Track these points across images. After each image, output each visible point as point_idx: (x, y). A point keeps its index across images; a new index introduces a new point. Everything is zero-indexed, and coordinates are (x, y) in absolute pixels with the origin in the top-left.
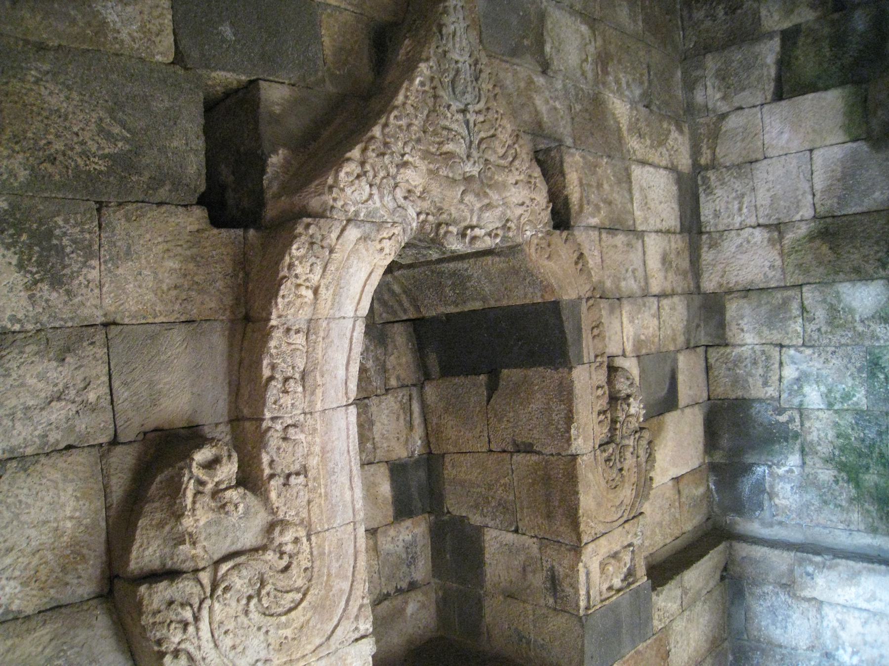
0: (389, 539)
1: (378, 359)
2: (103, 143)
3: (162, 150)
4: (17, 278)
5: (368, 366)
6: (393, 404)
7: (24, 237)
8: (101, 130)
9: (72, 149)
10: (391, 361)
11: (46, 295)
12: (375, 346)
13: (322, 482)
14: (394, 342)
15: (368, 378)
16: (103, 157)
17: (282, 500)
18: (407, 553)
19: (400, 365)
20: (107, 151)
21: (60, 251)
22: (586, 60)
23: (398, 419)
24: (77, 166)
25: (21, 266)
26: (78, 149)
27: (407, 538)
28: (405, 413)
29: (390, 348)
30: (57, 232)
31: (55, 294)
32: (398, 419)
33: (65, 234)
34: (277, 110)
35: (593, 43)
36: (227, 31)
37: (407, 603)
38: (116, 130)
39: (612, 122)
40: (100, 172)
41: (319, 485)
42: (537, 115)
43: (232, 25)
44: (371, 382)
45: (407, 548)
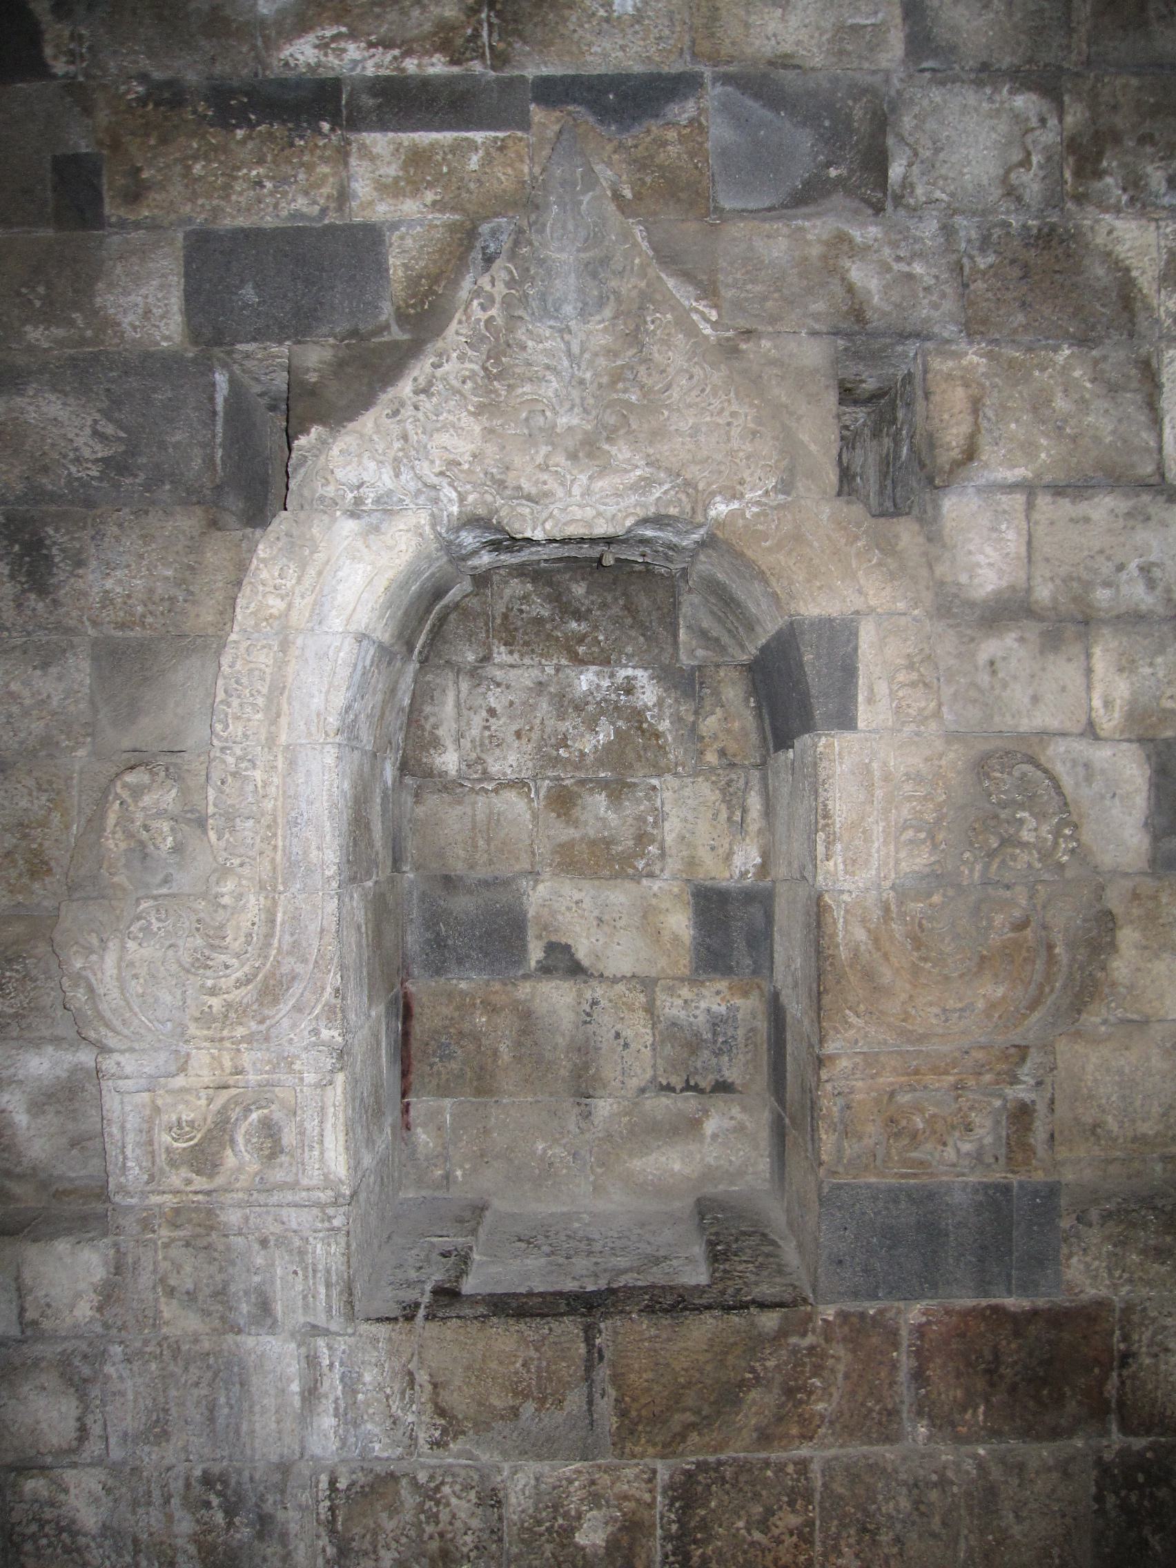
0: (680, 1002)
1: (680, 719)
2: (98, 447)
3: (162, 446)
4: (9, 589)
5: (661, 728)
6: (707, 792)
7: (17, 548)
8: (96, 433)
9: (65, 457)
10: (710, 724)
11: (33, 603)
12: (676, 700)
13: (280, 832)
14: (716, 693)
15: (660, 747)
16: (97, 460)
17: (222, 844)
18: (715, 1034)
19: (729, 731)
20: (100, 455)
21: (48, 558)
22: (1025, 163)
23: (715, 816)
24: (70, 474)
25: (12, 577)
26: (71, 455)
27: (715, 1008)
28: (730, 808)
29: (708, 703)
30: (48, 542)
31: (41, 604)
32: (715, 816)
33: (55, 543)
34: (313, 378)
35: (1053, 122)
36: (249, 293)
37: (706, 1112)
38: (110, 430)
39: (1100, 271)
40: (93, 478)
41: (275, 835)
42: (853, 297)
43: (257, 286)
44: (666, 753)
45: (714, 1024)
